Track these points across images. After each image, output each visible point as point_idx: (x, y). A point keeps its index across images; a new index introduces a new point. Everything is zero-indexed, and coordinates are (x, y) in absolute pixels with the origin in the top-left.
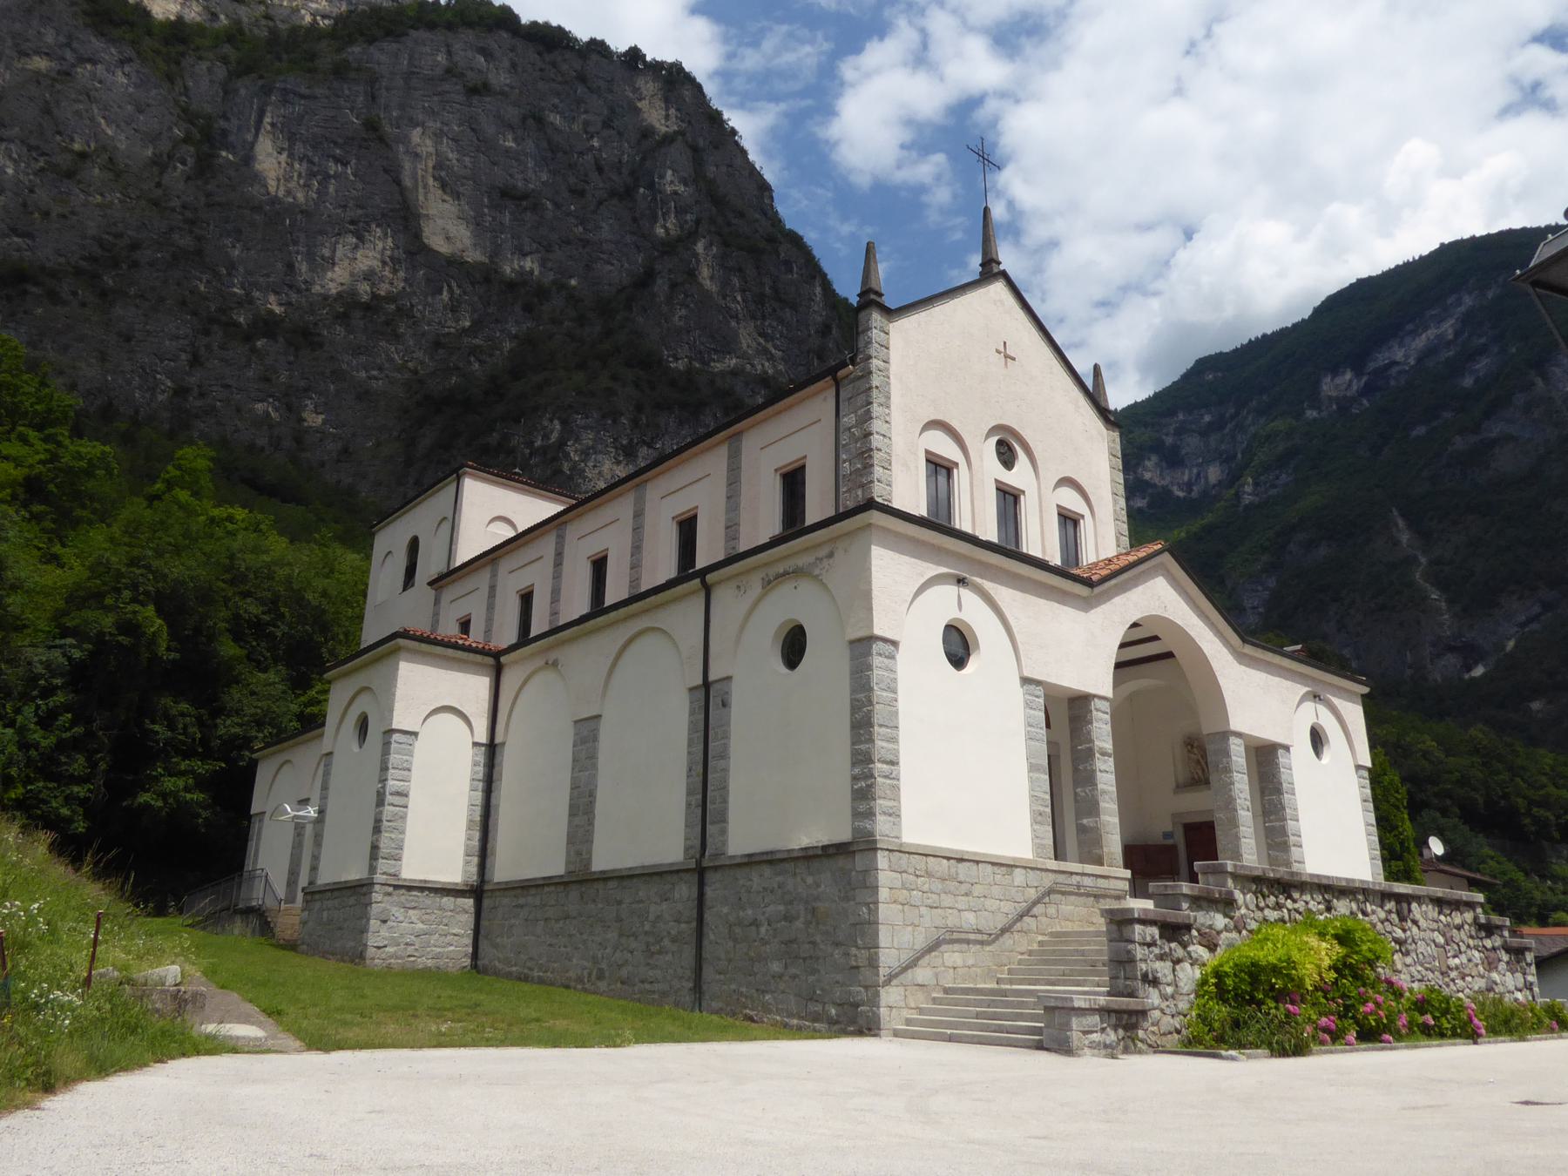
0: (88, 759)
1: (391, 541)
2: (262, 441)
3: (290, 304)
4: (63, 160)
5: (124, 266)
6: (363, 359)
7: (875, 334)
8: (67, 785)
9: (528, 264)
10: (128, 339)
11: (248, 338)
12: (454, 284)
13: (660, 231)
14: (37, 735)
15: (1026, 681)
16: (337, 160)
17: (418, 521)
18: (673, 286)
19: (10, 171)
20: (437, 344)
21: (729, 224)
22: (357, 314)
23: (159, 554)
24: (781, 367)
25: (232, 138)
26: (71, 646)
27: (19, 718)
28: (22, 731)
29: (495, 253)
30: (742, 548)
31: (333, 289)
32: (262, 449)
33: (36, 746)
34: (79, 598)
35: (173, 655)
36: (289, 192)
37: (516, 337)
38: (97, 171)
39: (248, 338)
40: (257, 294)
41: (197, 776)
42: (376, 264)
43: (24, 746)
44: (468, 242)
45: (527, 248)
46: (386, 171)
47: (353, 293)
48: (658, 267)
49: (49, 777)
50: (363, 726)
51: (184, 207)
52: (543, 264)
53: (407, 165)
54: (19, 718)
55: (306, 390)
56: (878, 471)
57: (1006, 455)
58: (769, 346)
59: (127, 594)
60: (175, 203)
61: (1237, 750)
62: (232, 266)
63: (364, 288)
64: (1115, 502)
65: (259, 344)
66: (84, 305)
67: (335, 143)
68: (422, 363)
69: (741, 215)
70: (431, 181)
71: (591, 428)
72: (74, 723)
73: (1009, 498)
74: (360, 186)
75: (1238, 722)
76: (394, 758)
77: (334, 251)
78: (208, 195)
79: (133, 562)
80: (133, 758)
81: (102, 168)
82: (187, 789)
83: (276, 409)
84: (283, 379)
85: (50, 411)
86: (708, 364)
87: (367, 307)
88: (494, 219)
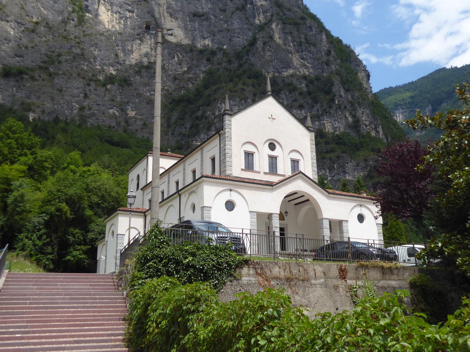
0: (52, 248)
1: (132, 176)
2: (113, 124)
3: (118, 70)
4: (30, 26)
5: (56, 63)
6: (148, 88)
7: (227, 122)
8: (47, 255)
9: (207, 42)
10: (61, 91)
11: (104, 85)
12: (179, 54)
13: (257, 22)
14: (37, 242)
15: (250, 212)
16: (129, 11)
17: (138, 170)
18: (264, 43)
19: (12, 33)
20: (175, 79)
21: (285, 15)
22: (143, 70)
23: (66, 187)
24: (311, 71)
25: (90, 8)
26: (45, 216)
27: (32, 238)
28: (33, 241)
29: (194, 40)
30: (186, 185)
31: (134, 62)
32: (114, 127)
33: (37, 245)
34: (46, 202)
35: (72, 216)
36: (113, 26)
37: (205, 72)
38: (42, 28)
39: (104, 85)
40: (105, 68)
41: (83, 251)
42: (149, 50)
43: (35, 245)
44: (182, 36)
45: (206, 36)
46: (148, 13)
47: (141, 62)
48: (257, 36)
49: (42, 253)
50: (113, 233)
51: (75, 38)
52: (212, 41)
53: (156, 9)
54: (32, 238)
55: (128, 103)
56: (227, 159)
57: (272, 146)
58: (306, 63)
59: (57, 200)
60: (72, 36)
61: (326, 224)
62: (95, 58)
63: (145, 60)
64: (312, 154)
65: (108, 87)
66: (43, 80)
67: (128, 4)
68: (170, 87)
69: (290, 10)
70: (166, 14)
71: (237, 105)
72: (47, 238)
73: (273, 160)
74: (139, 20)
75: (325, 216)
76: (119, 241)
77: (132, 47)
78: (84, 32)
79: (59, 191)
80: (64, 246)
81: (45, 27)
82: (80, 254)
83: (117, 111)
84: (119, 99)
85: (32, 144)
86: (281, 74)
87: (147, 67)
88: (192, 26)
